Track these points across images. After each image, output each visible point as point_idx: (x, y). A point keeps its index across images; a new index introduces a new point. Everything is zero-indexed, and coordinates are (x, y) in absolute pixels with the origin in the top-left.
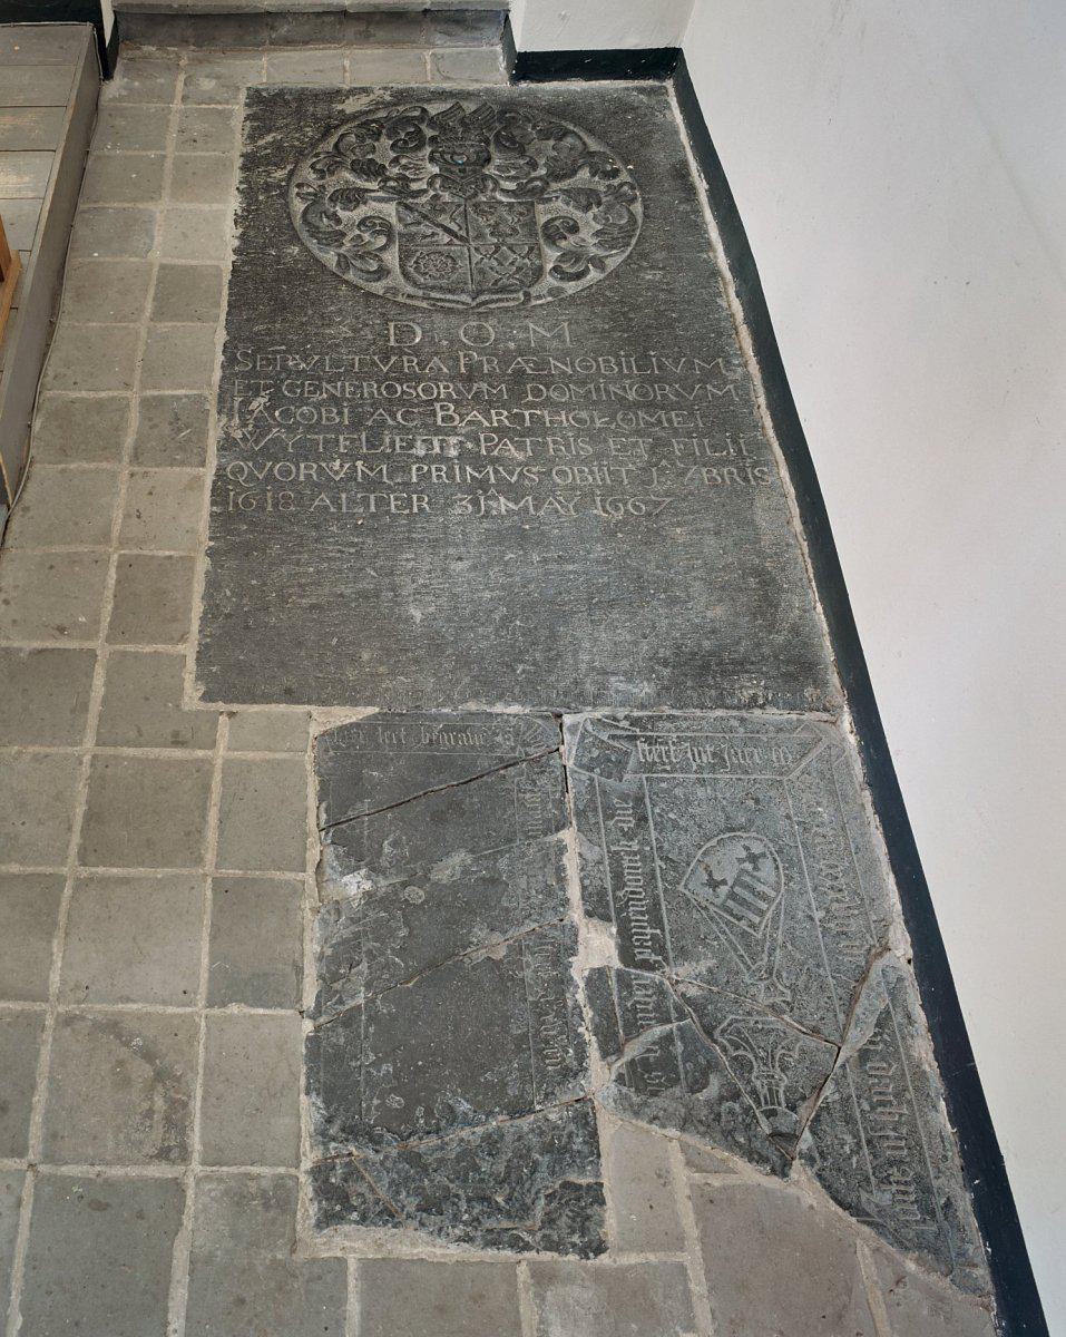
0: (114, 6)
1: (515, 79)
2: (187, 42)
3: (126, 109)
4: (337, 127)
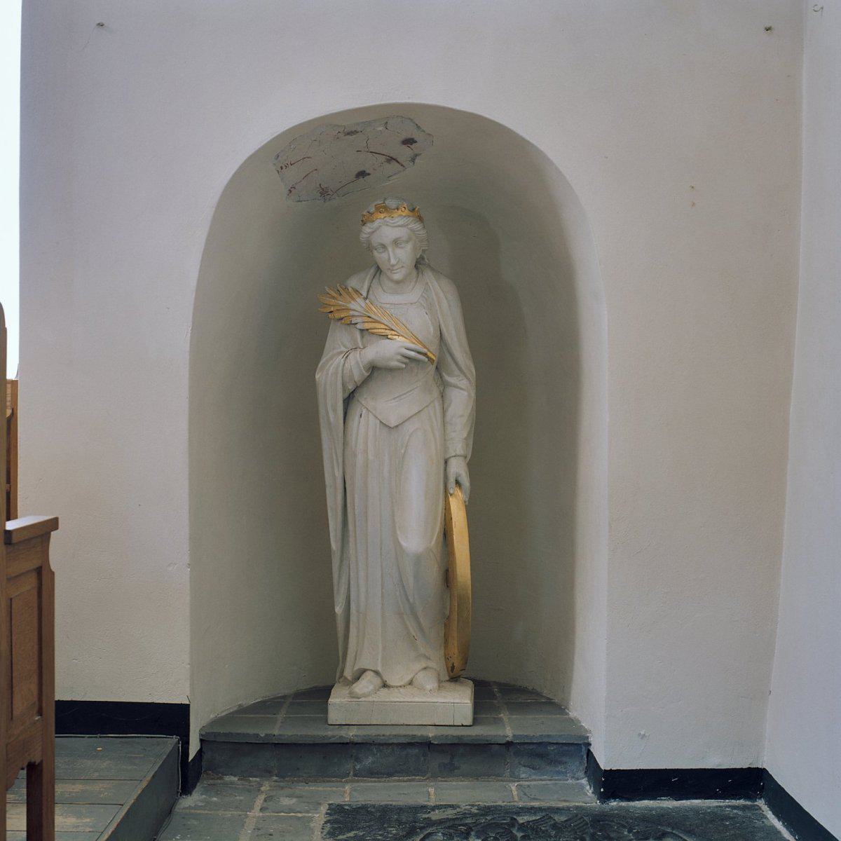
0: (201, 735)
1: (604, 797)
2: (270, 772)
3: (200, 814)
4: (421, 828)
